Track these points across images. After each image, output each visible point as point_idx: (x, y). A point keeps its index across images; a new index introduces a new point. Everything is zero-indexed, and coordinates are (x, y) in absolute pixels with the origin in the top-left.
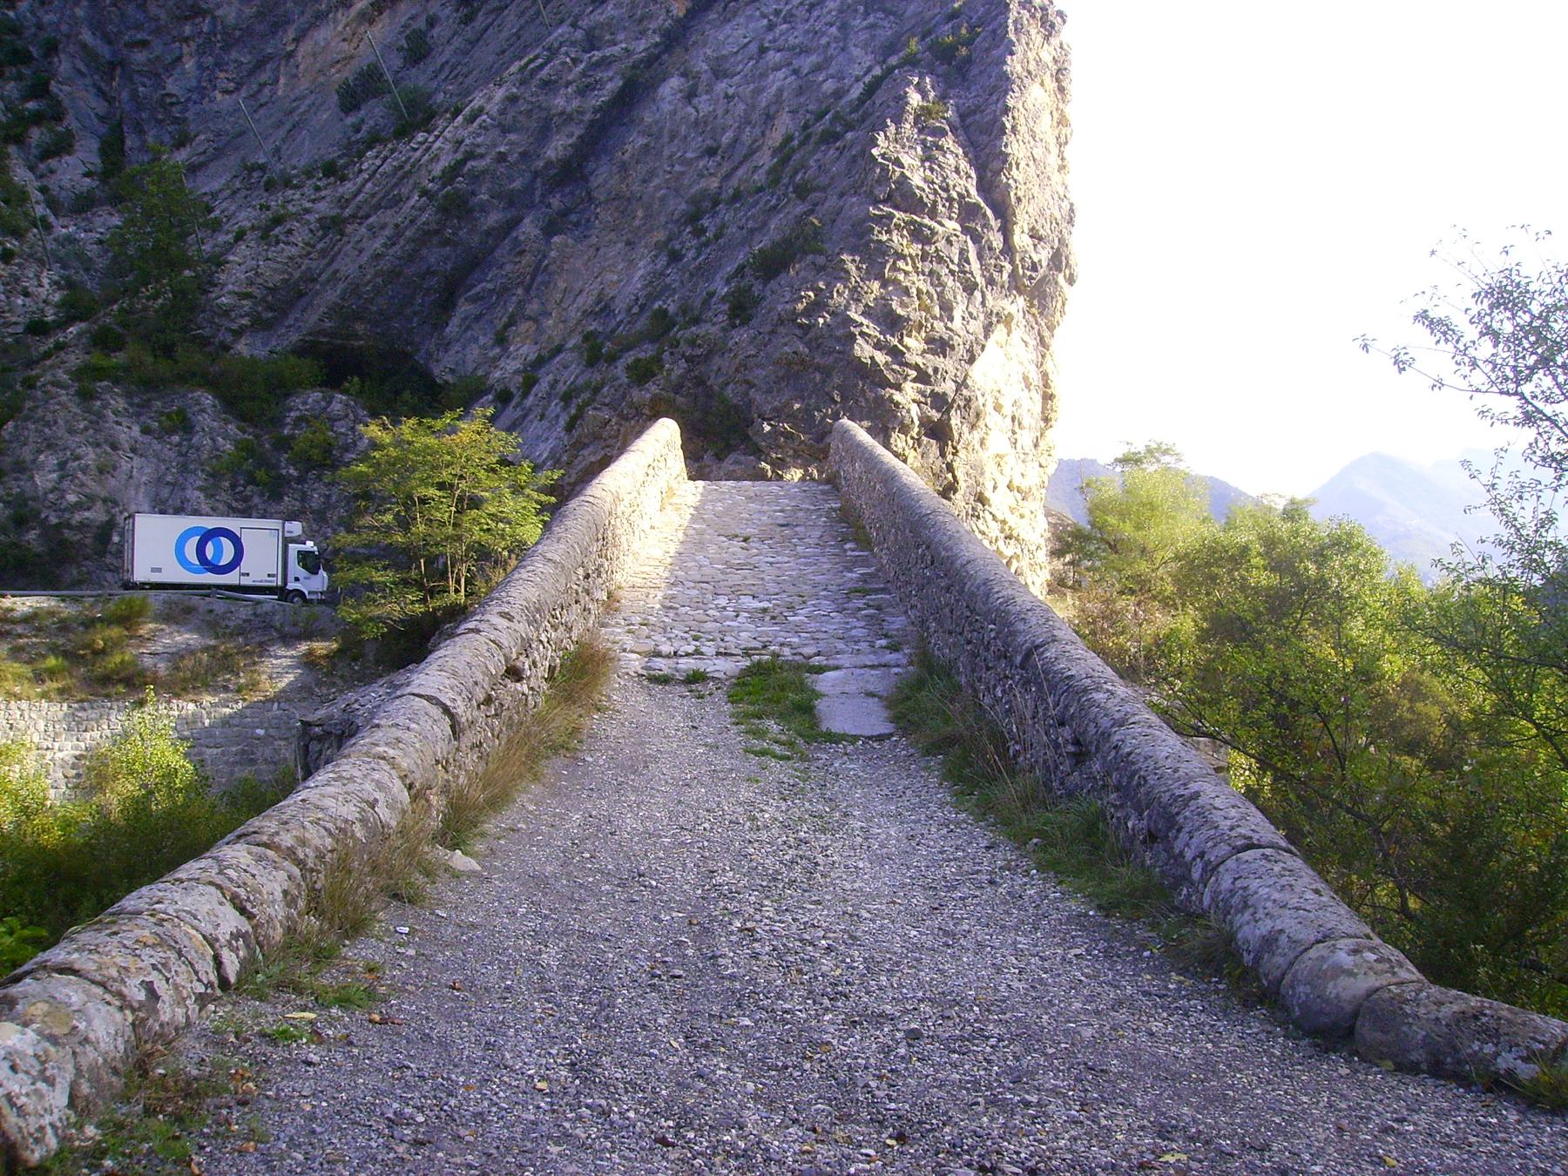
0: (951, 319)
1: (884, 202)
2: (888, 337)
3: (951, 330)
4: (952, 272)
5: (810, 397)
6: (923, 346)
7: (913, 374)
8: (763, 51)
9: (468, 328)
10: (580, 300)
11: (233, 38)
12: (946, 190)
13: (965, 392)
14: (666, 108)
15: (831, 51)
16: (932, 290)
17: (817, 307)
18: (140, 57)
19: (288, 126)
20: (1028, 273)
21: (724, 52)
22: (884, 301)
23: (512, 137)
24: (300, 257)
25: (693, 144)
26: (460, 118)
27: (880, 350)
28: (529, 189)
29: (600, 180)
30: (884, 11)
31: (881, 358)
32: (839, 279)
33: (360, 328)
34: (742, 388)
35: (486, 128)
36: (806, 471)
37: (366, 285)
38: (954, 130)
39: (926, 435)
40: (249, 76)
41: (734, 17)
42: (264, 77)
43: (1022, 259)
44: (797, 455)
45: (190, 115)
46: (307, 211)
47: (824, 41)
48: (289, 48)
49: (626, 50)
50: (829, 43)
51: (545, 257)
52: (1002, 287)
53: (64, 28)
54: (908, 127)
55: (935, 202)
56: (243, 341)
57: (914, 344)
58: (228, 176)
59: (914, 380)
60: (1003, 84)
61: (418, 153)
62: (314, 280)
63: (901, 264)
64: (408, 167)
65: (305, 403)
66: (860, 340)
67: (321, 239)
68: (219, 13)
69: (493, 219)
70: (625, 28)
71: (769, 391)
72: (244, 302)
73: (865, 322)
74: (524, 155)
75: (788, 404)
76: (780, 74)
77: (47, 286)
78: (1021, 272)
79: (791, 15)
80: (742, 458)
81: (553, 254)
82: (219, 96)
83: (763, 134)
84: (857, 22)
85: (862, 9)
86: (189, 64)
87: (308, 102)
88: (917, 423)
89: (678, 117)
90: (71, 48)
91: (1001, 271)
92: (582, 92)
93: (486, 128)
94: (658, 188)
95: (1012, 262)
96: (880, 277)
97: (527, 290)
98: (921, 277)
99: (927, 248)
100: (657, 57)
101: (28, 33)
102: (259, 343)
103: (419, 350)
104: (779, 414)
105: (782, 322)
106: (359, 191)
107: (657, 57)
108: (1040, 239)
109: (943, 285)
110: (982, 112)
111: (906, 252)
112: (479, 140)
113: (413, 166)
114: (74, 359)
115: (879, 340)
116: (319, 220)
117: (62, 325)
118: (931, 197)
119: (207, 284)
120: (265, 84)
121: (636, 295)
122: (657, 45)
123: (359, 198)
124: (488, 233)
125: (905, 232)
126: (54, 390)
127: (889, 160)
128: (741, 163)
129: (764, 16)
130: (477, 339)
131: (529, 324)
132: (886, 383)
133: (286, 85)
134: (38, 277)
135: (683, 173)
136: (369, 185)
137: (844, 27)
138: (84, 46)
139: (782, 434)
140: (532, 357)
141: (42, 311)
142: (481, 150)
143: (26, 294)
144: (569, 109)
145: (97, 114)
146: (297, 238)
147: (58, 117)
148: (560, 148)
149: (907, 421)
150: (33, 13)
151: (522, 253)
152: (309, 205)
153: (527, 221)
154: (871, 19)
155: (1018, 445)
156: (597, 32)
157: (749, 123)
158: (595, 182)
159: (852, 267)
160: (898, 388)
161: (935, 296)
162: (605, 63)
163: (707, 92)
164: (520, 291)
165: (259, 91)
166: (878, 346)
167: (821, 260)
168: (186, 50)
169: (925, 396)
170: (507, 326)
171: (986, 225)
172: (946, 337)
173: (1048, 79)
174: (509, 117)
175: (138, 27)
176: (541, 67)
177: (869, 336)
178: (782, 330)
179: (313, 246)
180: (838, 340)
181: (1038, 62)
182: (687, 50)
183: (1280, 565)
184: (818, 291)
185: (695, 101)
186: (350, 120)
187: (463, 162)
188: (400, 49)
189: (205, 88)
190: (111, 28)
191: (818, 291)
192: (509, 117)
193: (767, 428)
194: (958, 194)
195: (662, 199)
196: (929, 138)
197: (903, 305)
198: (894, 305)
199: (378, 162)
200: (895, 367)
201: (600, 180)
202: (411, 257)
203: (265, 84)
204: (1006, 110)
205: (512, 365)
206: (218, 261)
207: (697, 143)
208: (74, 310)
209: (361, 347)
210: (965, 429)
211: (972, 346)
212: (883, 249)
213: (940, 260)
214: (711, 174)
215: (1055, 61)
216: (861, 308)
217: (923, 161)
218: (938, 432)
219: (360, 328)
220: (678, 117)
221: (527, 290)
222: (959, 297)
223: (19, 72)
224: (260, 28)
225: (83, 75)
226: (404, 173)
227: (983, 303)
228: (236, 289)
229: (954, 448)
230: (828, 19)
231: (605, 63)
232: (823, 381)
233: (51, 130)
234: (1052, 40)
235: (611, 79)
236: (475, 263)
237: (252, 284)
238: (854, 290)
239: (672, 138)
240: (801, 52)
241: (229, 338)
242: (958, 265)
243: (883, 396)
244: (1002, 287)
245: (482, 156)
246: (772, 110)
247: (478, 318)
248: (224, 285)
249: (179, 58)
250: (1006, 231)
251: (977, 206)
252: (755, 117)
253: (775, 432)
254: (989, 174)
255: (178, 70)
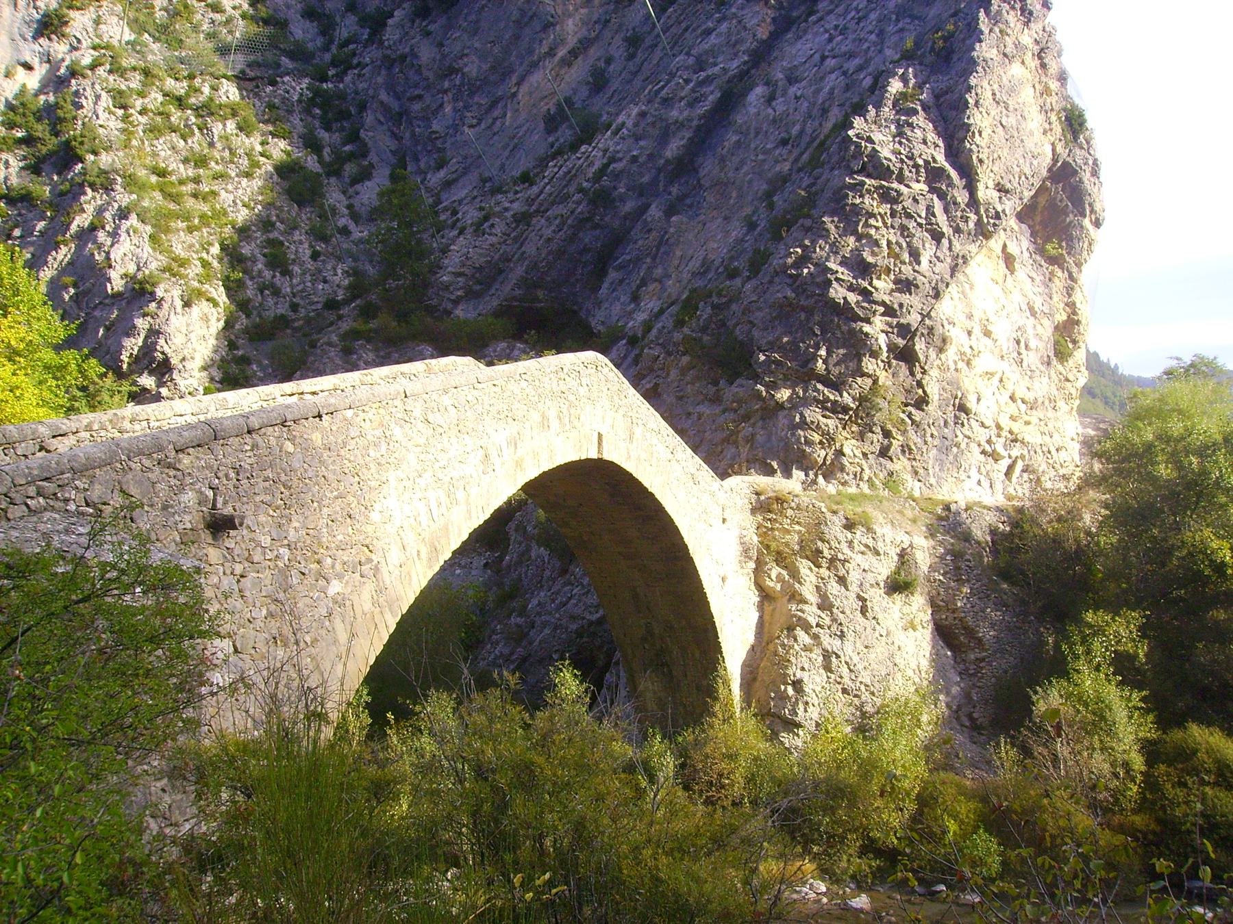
0: (919, 263)
1: (859, 172)
2: (860, 280)
3: (918, 272)
4: (920, 225)
5: (797, 332)
6: (892, 286)
7: (882, 309)
8: (823, 58)
9: (614, 290)
10: (690, 265)
11: (474, 88)
12: (911, 158)
13: (927, 322)
14: (752, 111)
15: (871, 54)
16: (901, 240)
17: (802, 261)
18: (416, 107)
19: (511, 147)
20: (992, 221)
21: (795, 63)
22: (857, 252)
23: (642, 143)
24: (499, 243)
25: (772, 138)
26: (609, 133)
27: (852, 291)
28: (654, 182)
29: (706, 170)
30: (910, 16)
31: (853, 298)
32: (821, 237)
33: (540, 294)
34: (746, 328)
35: (624, 139)
36: (794, 390)
37: (541, 262)
38: (925, 108)
39: (894, 358)
40: (486, 113)
41: (804, 34)
42: (496, 113)
43: (987, 210)
44: (786, 378)
45: (448, 145)
46: (506, 209)
47: (865, 47)
48: (513, 91)
49: (724, 69)
50: (869, 48)
51: (666, 233)
52: (969, 234)
53: (371, 92)
54: (887, 111)
55: (901, 169)
56: (460, 307)
57: (882, 286)
58: (470, 188)
59: (883, 315)
60: (971, 65)
61: (582, 160)
62: (509, 260)
63: (872, 221)
64: (574, 172)
65: (495, 351)
66: (835, 284)
67: (514, 230)
68: (466, 70)
69: (629, 206)
70: (723, 52)
71: (766, 329)
72: (459, 279)
73: (840, 269)
74: (651, 157)
75: (779, 339)
76: (833, 76)
77: (340, 275)
78: (985, 221)
79: (845, 28)
80: (744, 382)
81: (672, 230)
82: (466, 129)
83: (821, 125)
84: (891, 29)
85: (894, 17)
86: (448, 109)
87: (525, 128)
88: (885, 349)
89: (761, 117)
90: (375, 105)
91: (967, 222)
92: (691, 105)
93: (624, 139)
94: (746, 174)
95: (977, 213)
96: (854, 232)
97: (654, 258)
98: (892, 231)
99: (895, 207)
100: (748, 72)
101: (349, 98)
102: (471, 308)
103: (581, 309)
104: (773, 346)
105: (777, 273)
106: (541, 192)
107: (748, 72)
108: (1007, 192)
109: (911, 236)
110: (952, 92)
111: (876, 211)
112: (618, 148)
113: (577, 171)
114: (345, 326)
115: (852, 283)
116: (513, 216)
117: (347, 302)
118: (898, 165)
119: (436, 268)
120: (497, 118)
121: (722, 258)
122: (745, 63)
123: (541, 197)
124: (625, 218)
125: (875, 196)
126: (327, 348)
127: (862, 138)
128: (806, 149)
129: (826, 31)
130: (619, 299)
131: (656, 284)
132: (857, 318)
133: (511, 117)
134: (334, 269)
135: (764, 160)
136: (548, 187)
137: (881, 34)
138: (382, 102)
139: (773, 362)
140: (656, 310)
141: (335, 292)
142: (620, 155)
143: (325, 281)
144: (681, 118)
145: (391, 151)
146: (497, 230)
147: (364, 155)
148: (675, 149)
149: (875, 348)
150: (354, 83)
151: (649, 231)
152: (507, 205)
153: (653, 206)
154: (900, 25)
155: (1025, 364)
156: (704, 58)
157: (811, 117)
158: (702, 173)
159: (831, 227)
160: (868, 321)
161: (904, 245)
162: (708, 81)
163: (783, 96)
164: (648, 260)
165: (493, 123)
166: (851, 288)
167: (808, 222)
168: (446, 99)
169: (891, 327)
170: (639, 287)
171: (951, 184)
172: (911, 278)
173: (1028, 58)
174: (641, 128)
175: (416, 86)
176: (663, 87)
177: (843, 281)
178: (777, 280)
179: (509, 235)
180: (818, 285)
181: (1017, 45)
182: (770, 64)
183: (1175, 460)
184: (804, 248)
185: (774, 103)
186: (551, 139)
187: (606, 166)
188: (588, 83)
189: (457, 125)
190: (399, 89)
191: (804, 248)
192: (641, 128)
193: (762, 358)
194: (924, 160)
195: (750, 182)
196: (903, 118)
197: (874, 254)
198: (865, 254)
199: (556, 170)
200: (865, 304)
201: (706, 170)
202: (572, 239)
203: (497, 118)
204: (969, 89)
205: (641, 317)
206: (445, 251)
207: (776, 135)
208: (357, 289)
209: (541, 308)
210: (932, 353)
211: (937, 284)
212: (857, 210)
213: (909, 216)
214: (784, 160)
215: (1037, 42)
216: (839, 259)
217: (894, 137)
218: (906, 356)
219: (540, 294)
220: (761, 117)
221: (654, 258)
222: (927, 245)
223: (342, 125)
224: (492, 78)
225: (381, 123)
226: (570, 177)
227: (950, 249)
228: (453, 270)
229: (922, 368)
230: (870, 28)
231: (708, 81)
232: (808, 320)
233: (359, 165)
234: (1032, 25)
235: (712, 93)
236: (617, 241)
237: (464, 266)
238: (833, 245)
239: (757, 134)
240: (851, 56)
241: (449, 306)
242: (926, 219)
243: (854, 329)
244: (969, 234)
245: (621, 160)
246: (827, 105)
247: (621, 281)
248: (447, 267)
249: (441, 105)
250: (971, 187)
251: (942, 170)
252: (815, 112)
253: (769, 361)
254: (956, 142)
255: (441, 113)
